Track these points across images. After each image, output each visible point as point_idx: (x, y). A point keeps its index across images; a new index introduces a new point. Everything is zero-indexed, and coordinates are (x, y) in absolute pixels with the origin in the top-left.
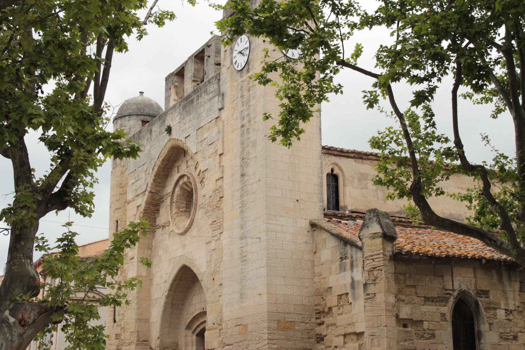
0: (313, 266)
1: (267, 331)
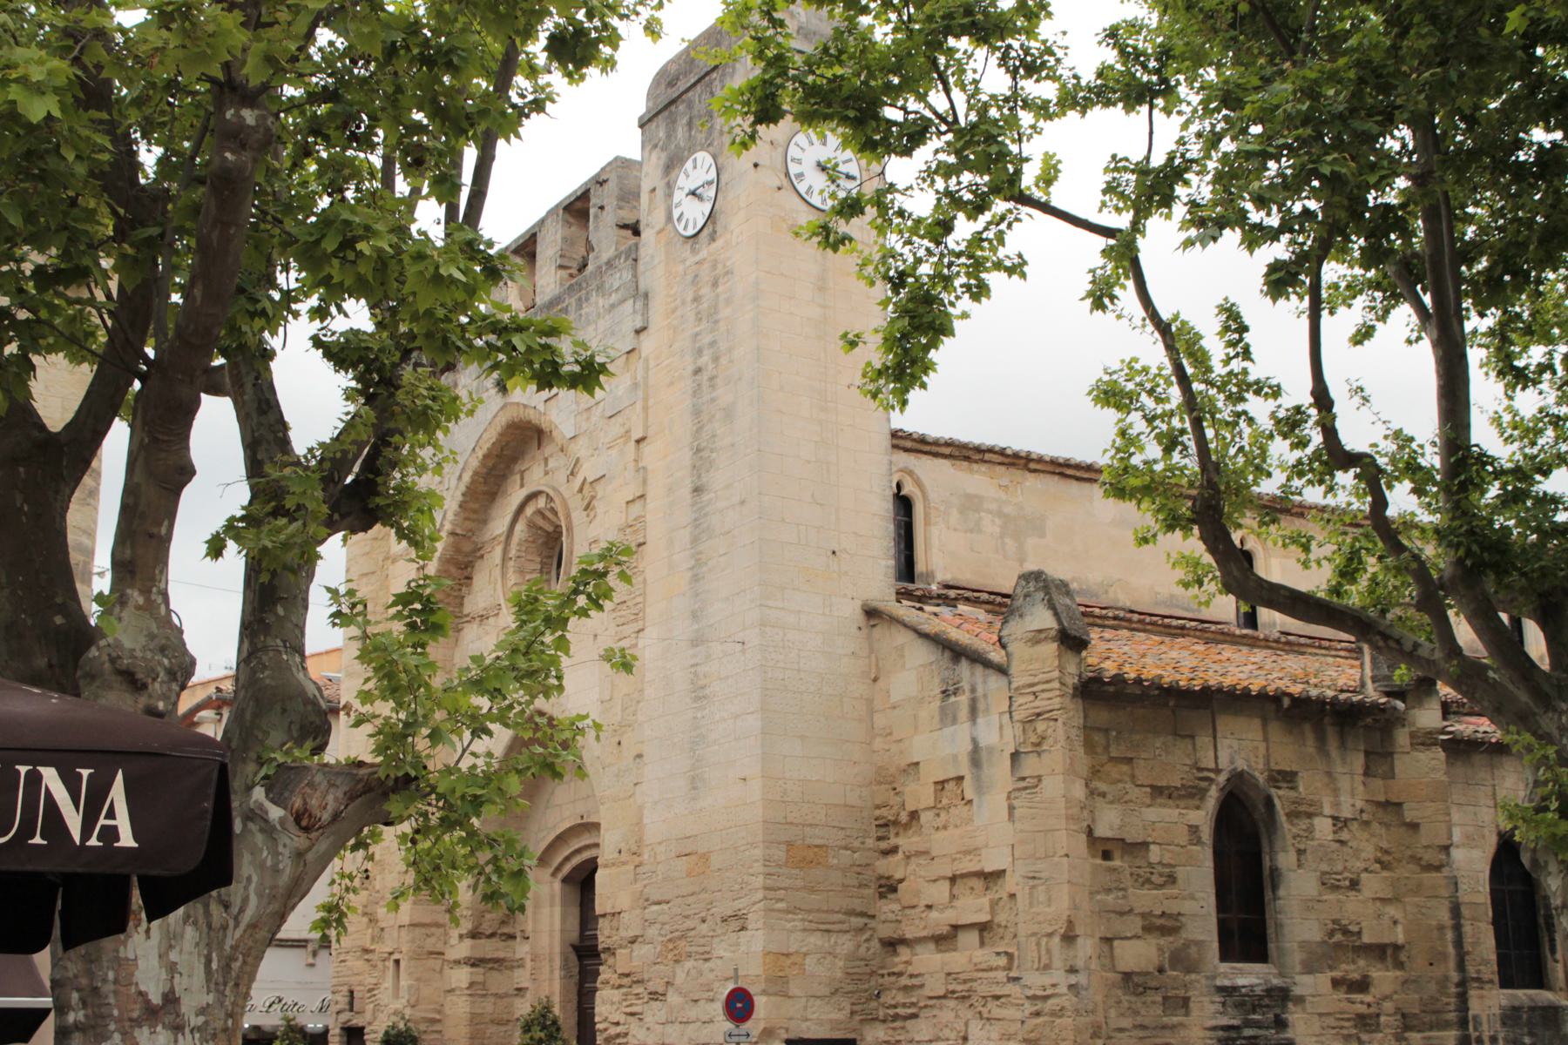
0: (871, 712)
1: (761, 869)
